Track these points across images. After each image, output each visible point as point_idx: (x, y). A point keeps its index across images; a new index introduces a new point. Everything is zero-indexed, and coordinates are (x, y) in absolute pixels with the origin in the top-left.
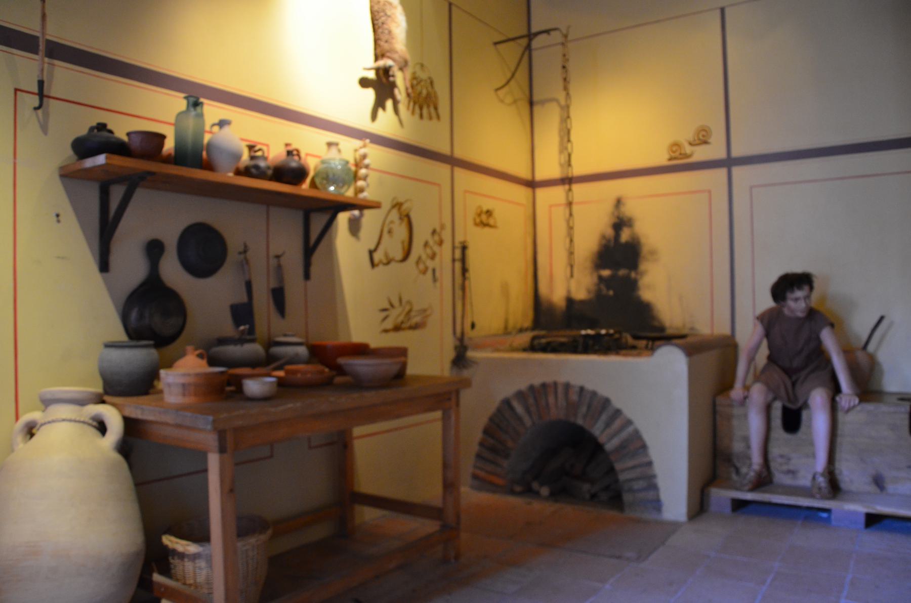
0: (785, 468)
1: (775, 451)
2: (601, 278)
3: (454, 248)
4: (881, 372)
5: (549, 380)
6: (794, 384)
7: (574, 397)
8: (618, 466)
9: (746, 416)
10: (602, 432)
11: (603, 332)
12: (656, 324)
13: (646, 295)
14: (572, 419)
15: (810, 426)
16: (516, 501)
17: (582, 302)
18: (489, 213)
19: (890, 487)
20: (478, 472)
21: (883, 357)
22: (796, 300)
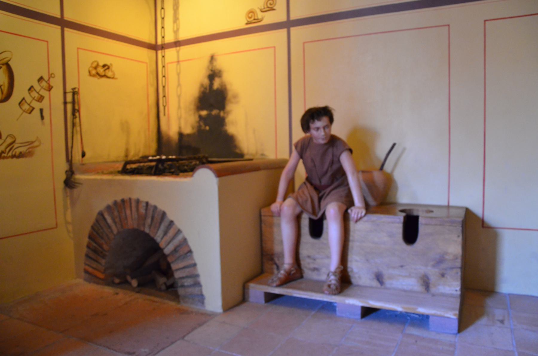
0: (312, 266)
1: (304, 252)
2: (200, 117)
3: (65, 93)
4: (396, 188)
5: (126, 197)
6: (320, 199)
7: (142, 211)
8: (174, 267)
9: (279, 226)
10: (162, 239)
11: (164, 157)
12: (237, 151)
13: (231, 129)
14: (142, 229)
15: (327, 233)
16: (108, 290)
17: (188, 135)
18: (106, 67)
19: (388, 283)
20: (88, 268)
21: (398, 176)
22: (318, 129)
